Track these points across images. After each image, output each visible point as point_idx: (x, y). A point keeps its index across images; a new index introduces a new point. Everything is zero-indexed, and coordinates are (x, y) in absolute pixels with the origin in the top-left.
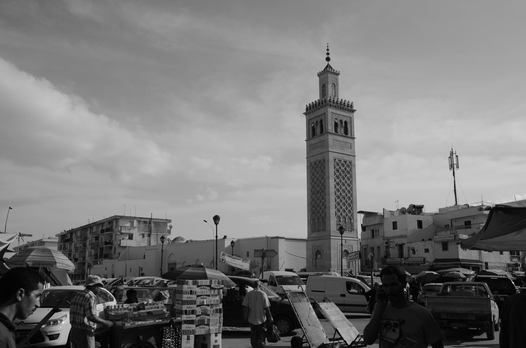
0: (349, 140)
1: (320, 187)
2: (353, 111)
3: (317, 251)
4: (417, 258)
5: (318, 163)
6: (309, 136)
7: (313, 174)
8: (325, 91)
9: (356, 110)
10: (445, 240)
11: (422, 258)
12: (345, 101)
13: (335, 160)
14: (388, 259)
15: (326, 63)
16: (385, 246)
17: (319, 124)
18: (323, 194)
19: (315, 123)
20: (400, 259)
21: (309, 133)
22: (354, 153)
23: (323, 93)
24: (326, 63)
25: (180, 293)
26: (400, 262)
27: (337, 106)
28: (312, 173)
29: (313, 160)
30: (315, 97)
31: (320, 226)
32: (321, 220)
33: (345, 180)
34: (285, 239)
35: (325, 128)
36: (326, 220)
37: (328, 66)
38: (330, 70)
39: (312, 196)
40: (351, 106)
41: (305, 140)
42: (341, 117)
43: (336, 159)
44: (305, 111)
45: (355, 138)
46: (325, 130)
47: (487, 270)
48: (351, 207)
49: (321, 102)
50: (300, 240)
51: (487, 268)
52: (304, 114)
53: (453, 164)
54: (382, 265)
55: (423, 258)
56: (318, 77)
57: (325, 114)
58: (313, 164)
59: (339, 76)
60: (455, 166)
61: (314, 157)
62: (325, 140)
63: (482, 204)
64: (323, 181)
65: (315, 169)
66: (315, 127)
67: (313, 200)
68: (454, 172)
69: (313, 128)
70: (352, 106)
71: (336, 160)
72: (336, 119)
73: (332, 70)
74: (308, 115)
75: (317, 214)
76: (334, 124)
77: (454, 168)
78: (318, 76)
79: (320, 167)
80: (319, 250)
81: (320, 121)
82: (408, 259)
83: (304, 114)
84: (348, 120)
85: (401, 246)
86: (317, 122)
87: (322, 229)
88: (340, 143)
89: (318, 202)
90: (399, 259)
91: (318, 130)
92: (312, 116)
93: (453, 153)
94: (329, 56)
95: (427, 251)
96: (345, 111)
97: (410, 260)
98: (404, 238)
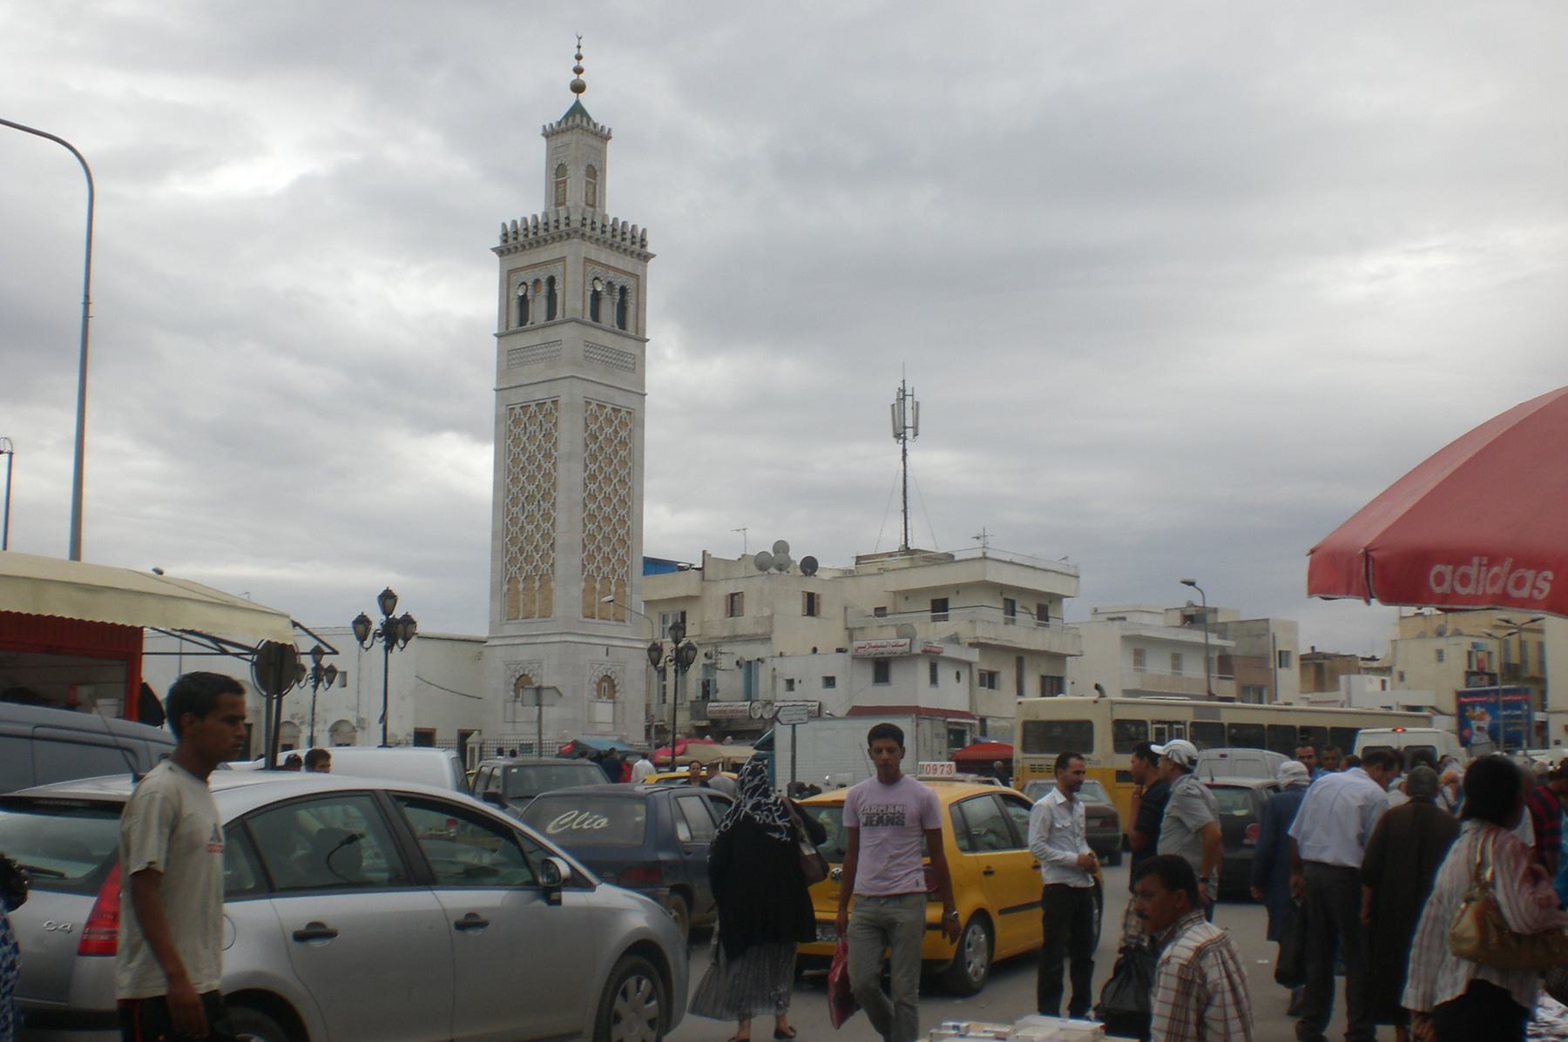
0: (629, 346)
1: (539, 482)
2: (647, 257)
3: (524, 675)
4: (732, 704)
5: (533, 408)
6: (507, 321)
7: (516, 441)
8: (565, 187)
9: (654, 256)
10: (883, 653)
11: (814, 704)
12: (624, 223)
13: (588, 403)
14: (713, 704)
15: (572, 98)
16: (704, 665)
17: (544, 289)
18: (544, 505)
19: (530, 284)
20: (749, 703)
21: (508, 314)
22: (643, 385)
23: (557, 191)
24: (572, 98)
25: (1466, 697)
26: (748, 714)
27: (602, 240)
28: (512, 438)
29: (518, 397)
30: (530, 204)
31: (533, 602)
32: (537, 584)
33: (613, 467)
34: (419, 637)
35: (564, 305)
36: (553, 584)
37: (577, 110)
38: (585, 123)
39: (508, 509)
40: (643, 240)
41: (495, 335)
42: (611, 273)
43: (608, 405)
44: (498, 243)
45: (648, 340)
46: (564, 309)
47: (984, 740)
48: (626, 549)
49: (552, 223)
50: (464, 640)
51: (984, 733)
52: (494, 250)
53: (905, 428)
54: (691, 720)
55: (817, 704)
56: (544, 139)
57: (564, 261)
58: (518, 410)
59: (609, 142)
60: (909, 433)
61: (521, 390)
62: (560, 341)
63: (984, 553)
64: (622, 492)
65: (523, 426)
66: (529, 298)
67: (514, 521)
68: (904, 451)
69: (523, 301)
70: (644, 243)
71: (590, 403)
72: (596, 278)
73: (588, 124)
74: (506, 257)
75: (524, 565)
76: (589, 294)
77: (905, 439)
78: (543, 135)
79: (541, 422)
80: (527, 675)
81: (548, 280)
82: (773, 704)
83: (494, 250)
84: (630, 284)
85: (749, 668)
86: (537, 282)
87: (540, 610)
88: (603, 353)
89: (529, 528)
90: (746, 703)
91: (538, 309)
92: (522, 260)
93: (904, 395)
94: (582, 77)
95: (830, 682)
96: (622, 255)
97: (711, 709)
98: (763, 644)
